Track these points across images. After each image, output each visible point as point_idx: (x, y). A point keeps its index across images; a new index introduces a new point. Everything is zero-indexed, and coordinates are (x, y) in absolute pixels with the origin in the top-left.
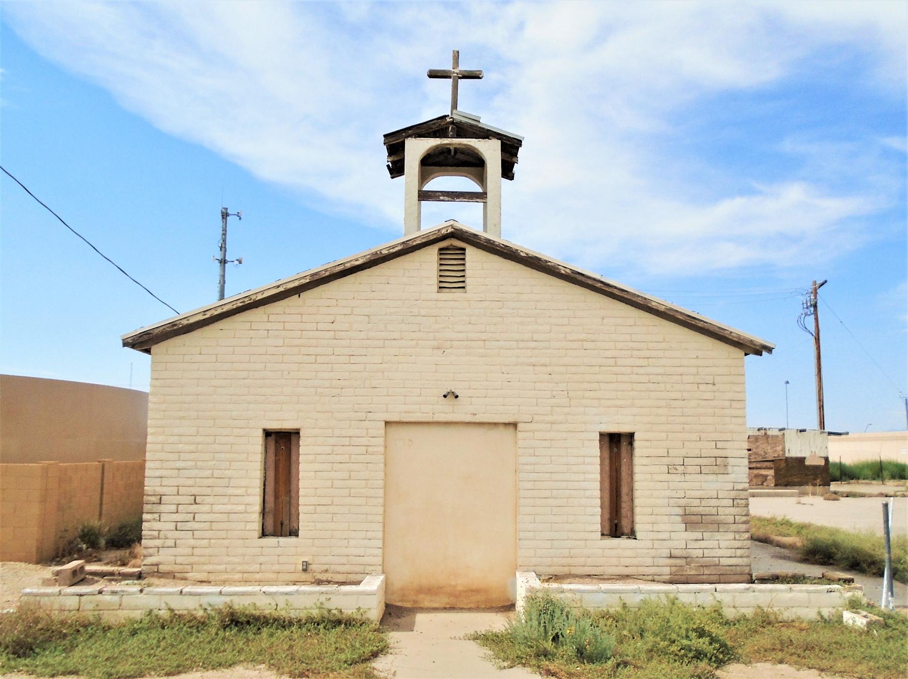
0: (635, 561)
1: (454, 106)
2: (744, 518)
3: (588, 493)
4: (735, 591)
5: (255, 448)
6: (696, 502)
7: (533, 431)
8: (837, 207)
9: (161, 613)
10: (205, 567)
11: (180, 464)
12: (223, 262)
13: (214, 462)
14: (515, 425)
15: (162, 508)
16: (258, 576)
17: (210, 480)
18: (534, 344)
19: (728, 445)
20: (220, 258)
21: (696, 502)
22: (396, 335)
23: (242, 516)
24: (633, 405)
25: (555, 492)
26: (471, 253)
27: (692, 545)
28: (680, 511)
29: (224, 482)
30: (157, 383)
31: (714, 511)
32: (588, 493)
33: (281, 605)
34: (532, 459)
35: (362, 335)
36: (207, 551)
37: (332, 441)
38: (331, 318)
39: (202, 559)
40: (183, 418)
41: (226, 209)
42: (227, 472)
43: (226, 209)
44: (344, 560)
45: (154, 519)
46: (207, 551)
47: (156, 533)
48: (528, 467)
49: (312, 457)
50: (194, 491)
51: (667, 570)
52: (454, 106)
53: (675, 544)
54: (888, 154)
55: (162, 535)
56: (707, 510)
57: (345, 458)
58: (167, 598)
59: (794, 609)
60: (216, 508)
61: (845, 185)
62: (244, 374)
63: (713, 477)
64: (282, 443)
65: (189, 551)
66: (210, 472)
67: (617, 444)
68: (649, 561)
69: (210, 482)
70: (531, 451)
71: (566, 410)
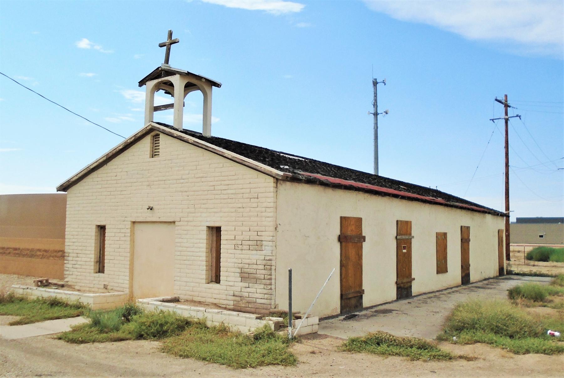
0: (218, 296)
1: (167, 61)
2: (269, 277)
3: (201, 258)
4: (213, 313)
5: (93, 232)
6: (247, 266)
7: (181, 226)
11: (74, 240)
12: (376, 114)
18: (182, 181)
19: (263, 233)
20: (373, 112)
21: (247, 266)
22: (135, 180)
24: (221, 212)
25: (188, 257)
26: (162, 136)
27: (243, 290)
28: (239, 270)
31: (254, 271)
32: (201, 258)
34: (180, 240)
37: (115, 230)
41: (376, 79)
43: (376, 79)
44: (117, 285)
48: (178, 244)
52: (167, 61)
56: (252, 271)
59: (239, 327)
63: (255, 252)
68: (224, 297)
70: (180, 236)
71: (194, 214)
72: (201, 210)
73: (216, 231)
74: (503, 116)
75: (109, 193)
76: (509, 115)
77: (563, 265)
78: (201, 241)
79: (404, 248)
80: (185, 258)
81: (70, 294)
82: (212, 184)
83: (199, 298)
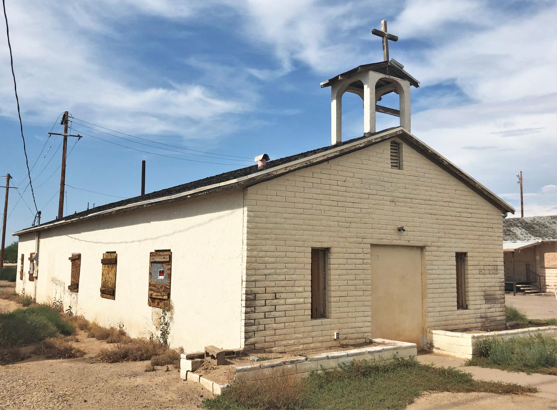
3: (452, 285)
8: (222, 106)
9: (319, 372)
10: (283, 343)
11: (266, 272)
13: (286, 270)
14: (422, 248)
15: (257, 303)
16: (312, 345)
17: (284, 282)
18: (431, 202)
22: (374, 192)
23: (302, 305)
28: (483, 293)
29: (291, 283)
30: (251, 214)
33: (377, 359)
34: (431, 267)
35: (359, 190)
36: (283, 331)
37: (347, 256)
38: (344, 179)
39: (281, 337)
40: (267, 239)
42: (293, 276)
45: (252, 311)
46: (283, 331)
47: (252, 321)
49: (337, 266)
50: (275, 290)
51: (480, 324)
53: (482, 311)
54: (252, 79)
55: (256, 323)
57: (353, 267)
58: (320, 362)
60: (289, 301)
61: (226, 93)
62: (301, 211)
64: (320, 256)
65: (272, 332)
66: (284, 276)
67: (461, 257)
69: (283, 283)
72: (450, 235)
73: (461, 257)
74: (62, 132)
75: (335, 203)
76: (68, 133)
77: (1, 289)
78: (452, 267)
79: (161, 273)
80: (437, 286)
81: (379, 351)
82: (459, 210)
83: (453, 326)
